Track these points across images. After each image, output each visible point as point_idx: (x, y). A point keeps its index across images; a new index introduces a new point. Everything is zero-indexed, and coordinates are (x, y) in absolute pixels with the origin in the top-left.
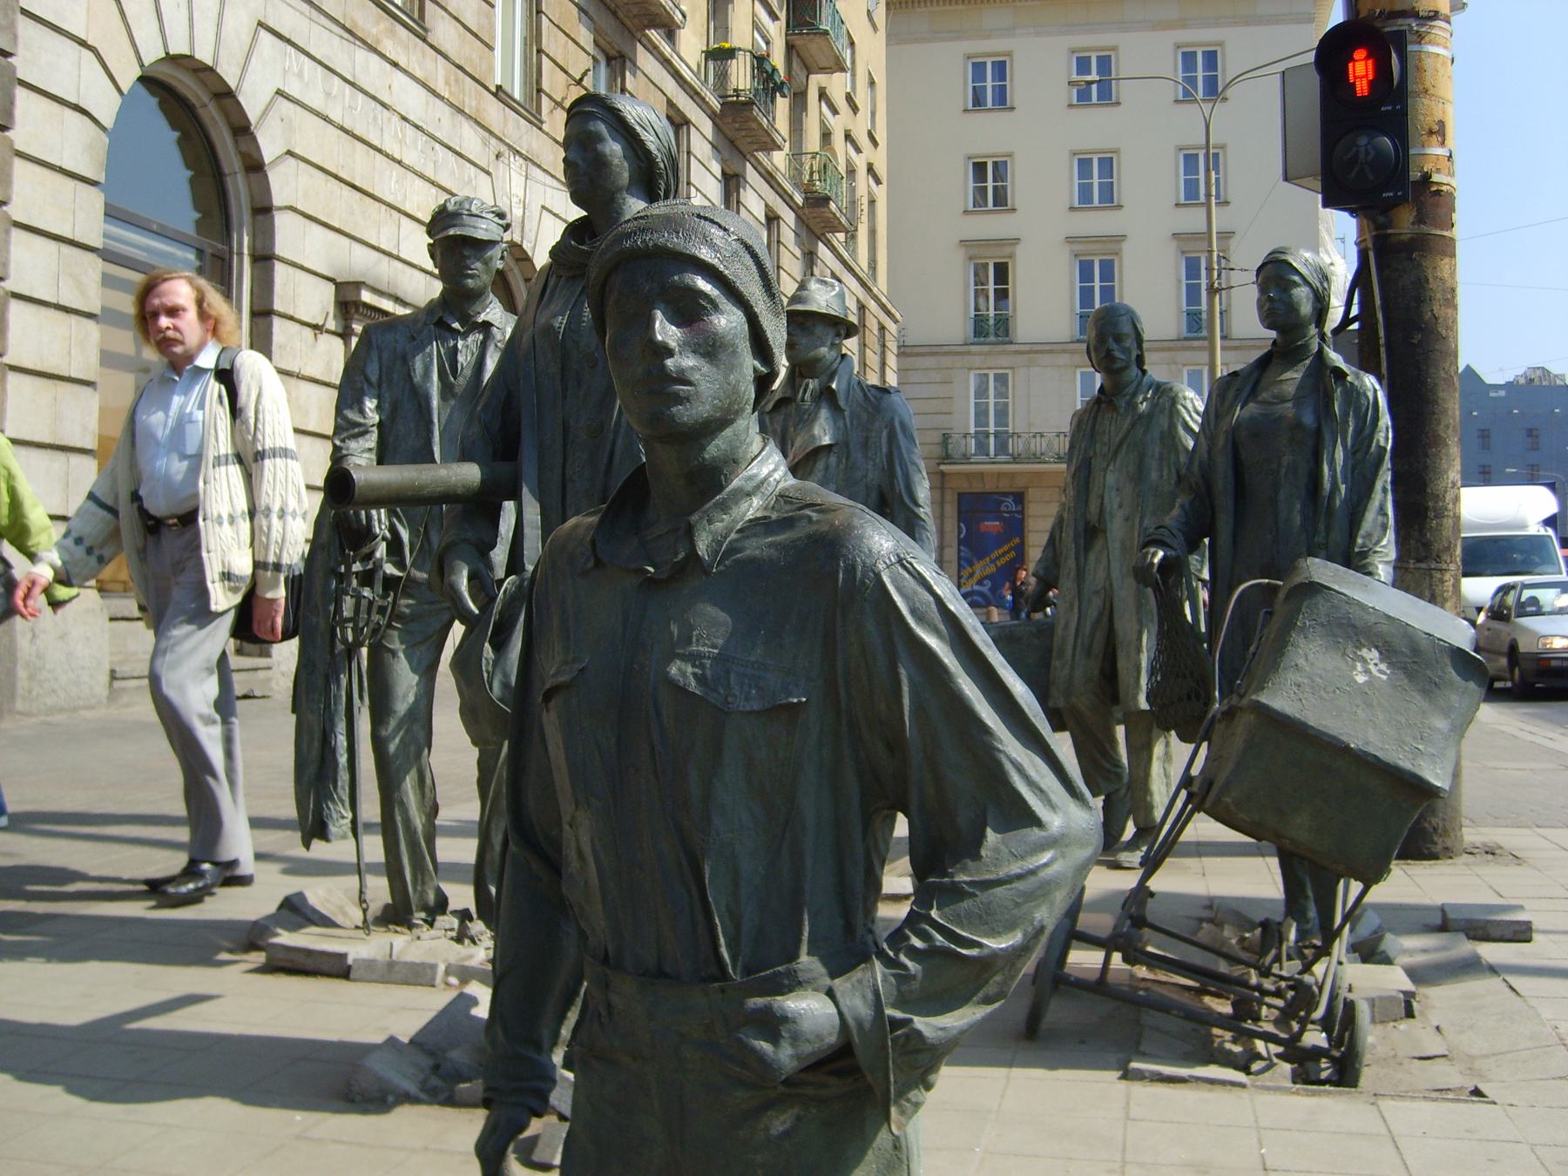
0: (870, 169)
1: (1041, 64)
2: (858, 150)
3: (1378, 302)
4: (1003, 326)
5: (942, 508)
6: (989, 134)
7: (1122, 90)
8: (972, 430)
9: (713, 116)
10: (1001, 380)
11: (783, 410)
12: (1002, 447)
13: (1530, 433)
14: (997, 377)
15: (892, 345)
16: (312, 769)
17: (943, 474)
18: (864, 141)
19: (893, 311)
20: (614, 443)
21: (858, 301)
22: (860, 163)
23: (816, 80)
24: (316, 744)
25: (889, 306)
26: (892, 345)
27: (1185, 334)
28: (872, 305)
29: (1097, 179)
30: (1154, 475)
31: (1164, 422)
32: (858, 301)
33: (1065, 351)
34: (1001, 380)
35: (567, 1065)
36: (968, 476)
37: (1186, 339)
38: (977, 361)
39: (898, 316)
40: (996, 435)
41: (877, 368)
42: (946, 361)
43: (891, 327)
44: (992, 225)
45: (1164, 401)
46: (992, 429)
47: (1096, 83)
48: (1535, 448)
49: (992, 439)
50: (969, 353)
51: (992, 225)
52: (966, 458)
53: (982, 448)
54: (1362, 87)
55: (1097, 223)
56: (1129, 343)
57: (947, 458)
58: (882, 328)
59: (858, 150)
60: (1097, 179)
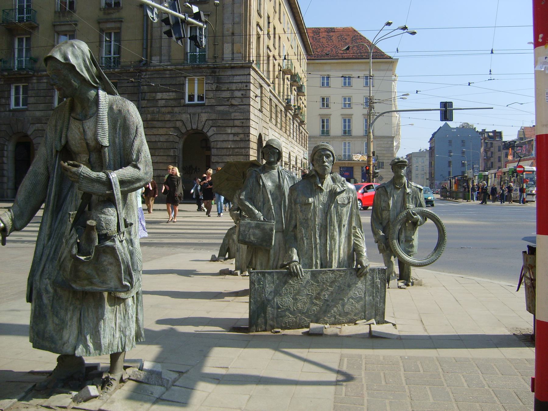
0: (274, 57)
1: (336, 82)
2: (270, 51)
4: (328, 133)
6: (325, 92)
7: (353, 106)
9: (284, 107)
13: (463, 141)
18: (277, 57)
22: (271, 54)
23: (286, 76)
29: (348, 103)
35: (541, 38)
38: (322, 139)
42: (316, 139)
44: (325, 111)
47: (347, 80)
48: (463, 146)
51: (325, 111)
55: (347, 111)
59: (270, 51)
60: (348, 103)
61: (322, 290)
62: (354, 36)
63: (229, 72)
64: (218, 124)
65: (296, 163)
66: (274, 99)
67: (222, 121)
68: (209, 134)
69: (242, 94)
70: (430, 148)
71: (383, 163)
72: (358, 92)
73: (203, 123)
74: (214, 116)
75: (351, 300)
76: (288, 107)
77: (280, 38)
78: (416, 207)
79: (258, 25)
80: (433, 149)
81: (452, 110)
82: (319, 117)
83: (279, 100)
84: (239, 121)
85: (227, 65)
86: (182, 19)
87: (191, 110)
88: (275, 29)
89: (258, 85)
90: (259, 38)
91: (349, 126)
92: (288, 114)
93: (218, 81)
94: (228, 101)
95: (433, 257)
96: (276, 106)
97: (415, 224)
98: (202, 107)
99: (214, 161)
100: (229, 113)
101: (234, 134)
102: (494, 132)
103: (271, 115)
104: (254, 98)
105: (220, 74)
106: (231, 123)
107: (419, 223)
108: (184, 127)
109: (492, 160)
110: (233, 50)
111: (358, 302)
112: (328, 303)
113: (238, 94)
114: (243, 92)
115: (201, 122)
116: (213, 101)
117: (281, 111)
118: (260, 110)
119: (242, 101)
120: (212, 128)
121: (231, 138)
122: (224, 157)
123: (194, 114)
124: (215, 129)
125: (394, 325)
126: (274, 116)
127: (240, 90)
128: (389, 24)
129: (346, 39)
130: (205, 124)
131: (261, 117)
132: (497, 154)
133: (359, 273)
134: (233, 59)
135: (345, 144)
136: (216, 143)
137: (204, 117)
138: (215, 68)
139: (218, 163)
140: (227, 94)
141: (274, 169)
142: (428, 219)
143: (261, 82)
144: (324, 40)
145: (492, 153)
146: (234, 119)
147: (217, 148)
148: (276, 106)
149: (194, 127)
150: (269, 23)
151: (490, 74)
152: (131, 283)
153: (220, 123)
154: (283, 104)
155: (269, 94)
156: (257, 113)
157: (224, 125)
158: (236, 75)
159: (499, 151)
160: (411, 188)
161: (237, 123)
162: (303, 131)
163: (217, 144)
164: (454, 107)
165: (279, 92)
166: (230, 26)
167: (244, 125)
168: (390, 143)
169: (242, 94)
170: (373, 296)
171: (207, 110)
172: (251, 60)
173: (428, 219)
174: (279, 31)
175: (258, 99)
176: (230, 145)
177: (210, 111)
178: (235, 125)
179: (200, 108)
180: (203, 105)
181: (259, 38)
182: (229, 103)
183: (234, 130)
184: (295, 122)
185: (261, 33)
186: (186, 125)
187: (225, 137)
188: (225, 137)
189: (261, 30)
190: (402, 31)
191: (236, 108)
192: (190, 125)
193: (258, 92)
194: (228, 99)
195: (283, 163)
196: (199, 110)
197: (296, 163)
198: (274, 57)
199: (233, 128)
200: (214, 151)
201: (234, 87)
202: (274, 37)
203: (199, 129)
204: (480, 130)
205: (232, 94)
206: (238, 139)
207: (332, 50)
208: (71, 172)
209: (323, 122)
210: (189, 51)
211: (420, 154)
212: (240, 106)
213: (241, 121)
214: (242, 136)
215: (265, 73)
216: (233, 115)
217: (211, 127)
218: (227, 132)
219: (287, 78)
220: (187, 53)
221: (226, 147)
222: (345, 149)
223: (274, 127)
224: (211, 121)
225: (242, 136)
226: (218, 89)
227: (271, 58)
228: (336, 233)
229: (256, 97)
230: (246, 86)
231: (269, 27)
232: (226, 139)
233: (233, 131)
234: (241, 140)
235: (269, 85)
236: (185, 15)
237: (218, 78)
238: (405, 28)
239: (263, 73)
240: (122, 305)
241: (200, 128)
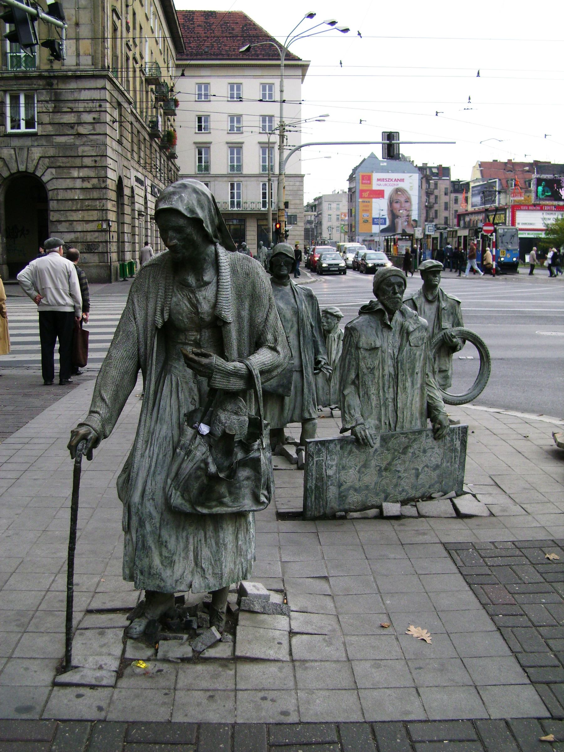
0: (134, 59)
2: (130, 50)
9: (149, 134)
22: (131, 54)
34: (239, 185)
61: (393, 459)
62: (246, 25)
63: (73, 85)
64: (58, 164)
65: (146, 208)
66: (136, 124)
67: (64, 159)
68: (45, 179)
69: (94, 119)
70: (350, 189)
71: (295, 217)
72: (252, 111)
73: (35, 162)
74: (51, 152)
75: (426, 469)
76: (154, 135)
77: (141, 28)
78: (453, 326)
79: (114, 10)
80: (353, 190)
81: (399, 144)
82: (194, 146)
83: (142, 125)
84: (90, 159)
85: (70, 74)
86: (31, 14)
87: (16, 142)
88: (134, 14)
89: (115, 105)
90: (115, 29)
91: (239, 160)
92: (154, 145)
93: (57, 100)
94: (72, 128)
95: (475, 392)
96: (138, 132)
97: (454, 348)
98: (34, 138)
99: (54, 220)
100: (73, 147)
101: (83, 179)
102: (440, 168)
103: (132, 147)
104: (111, 123)
105: (59, 87)
106: (78, 162)
107: (458, 347)
108: (5, 169)
109: (436, 207)
110: (77, 49)
111: (435, 469)
112: (400, 474)
113: (88, 118)
114: (96, 115)
115: (32, 161)
116: (50, 129)
117: (145, 139)
118: (120, 142)
119: (94, 129)
120: (50, 170)
121: (78, 184)
122: (69, 214)
123: (21, 149)
124: (53, 171)
125: (474, 496)
126: (136, 148)
127: (90, 112)
128: (311, 16)
129: (233, 29)
130: (38, 163)
131: (120, 151)
132: (443, 199)
133: (437, 435)
134: (78, 64)
135: (232, 185)
136: (55, 192)
137: (37, 153)
138: (50, 77)
139: (60, 222)
140: (70, 118)
141: (286, 285)
142: (467, 342)
143: (121, 99)
144: (200, 30)
145: (436, 197)
146: (83, 156)
147: (57, 200)
148: (138, 132)
149: (22, 168)
150: (127, 6)
151: (469, 102)
152: (269, 499)
153: (61, 162)
154: (148, 129)
155: (131, 118)
156: (115, 145)
157: (68, 165)
158: (85, 89)
159: (446, 194)
160: (447, 301)
161: (88, 161)
162: (173, 167)
163: (57, 194)
164: (401, 140)
165: (142, 112)
166: (73, 12)
167: (97, 165)
168: (298, 184)
169: (94, 119)
170: (451, 462)
171: (40, 142)
172: (106, 65)
173: (467, 342)
174: (140, 18)
175: (116, 125)
176: (77, 195)
177: (45, 144)
178: (84, 164)
179: (30, 138)
180: (35, 135)
181: (115, 29)
182: (74, 132)
183: (83, 173)
184: (162, 155)
185: (118, 23)
186: (10, 166)
187: (69, 183)
188: (69, 183)
189: (119, 18)
190: (330, 27)
191: (85, 139)
192: (14, 165)
193: (116, 114)
194: (71, 126)
195: (136, 213)
196: (28, 142)
197: (146, 208)
198: (134, 59)
199: (81, 170)
200: (53, 205)
201: (81, 107)
202: (134, 28)
203: (29, 171)
204: (420, 165)
205: (79, 117)
206: (89, 186)
207: (213, 46)
208: (202, 366)
209: (200, 153)
210: (8, 51)
211: (335, 198)
212: (91, 137)
213: (94, 158)
214: (95, 181)
215: (125, 84)
216: (80, 149)
217: (48, 168)
218: (72, 176)
219: (152, 90)
220: (6, 53)
221: (72, 198)
222: (232, 193)
223: (137, 166)
224: (47, 160)
225: (95, 181)
226: (57, 111)
227: (131, 61)
228: (409, 384)
229: (114, 122)
230: (100, 106)
231: (127, 13)
232: (71, 186)
233: (81, 175)
234: (94, 188)
235: (130, 103)
236: (36, 9)
237: (56, 94)
238: (333, 23)
239: (121, 84)
240: (243, 520)
241: (31, 170)
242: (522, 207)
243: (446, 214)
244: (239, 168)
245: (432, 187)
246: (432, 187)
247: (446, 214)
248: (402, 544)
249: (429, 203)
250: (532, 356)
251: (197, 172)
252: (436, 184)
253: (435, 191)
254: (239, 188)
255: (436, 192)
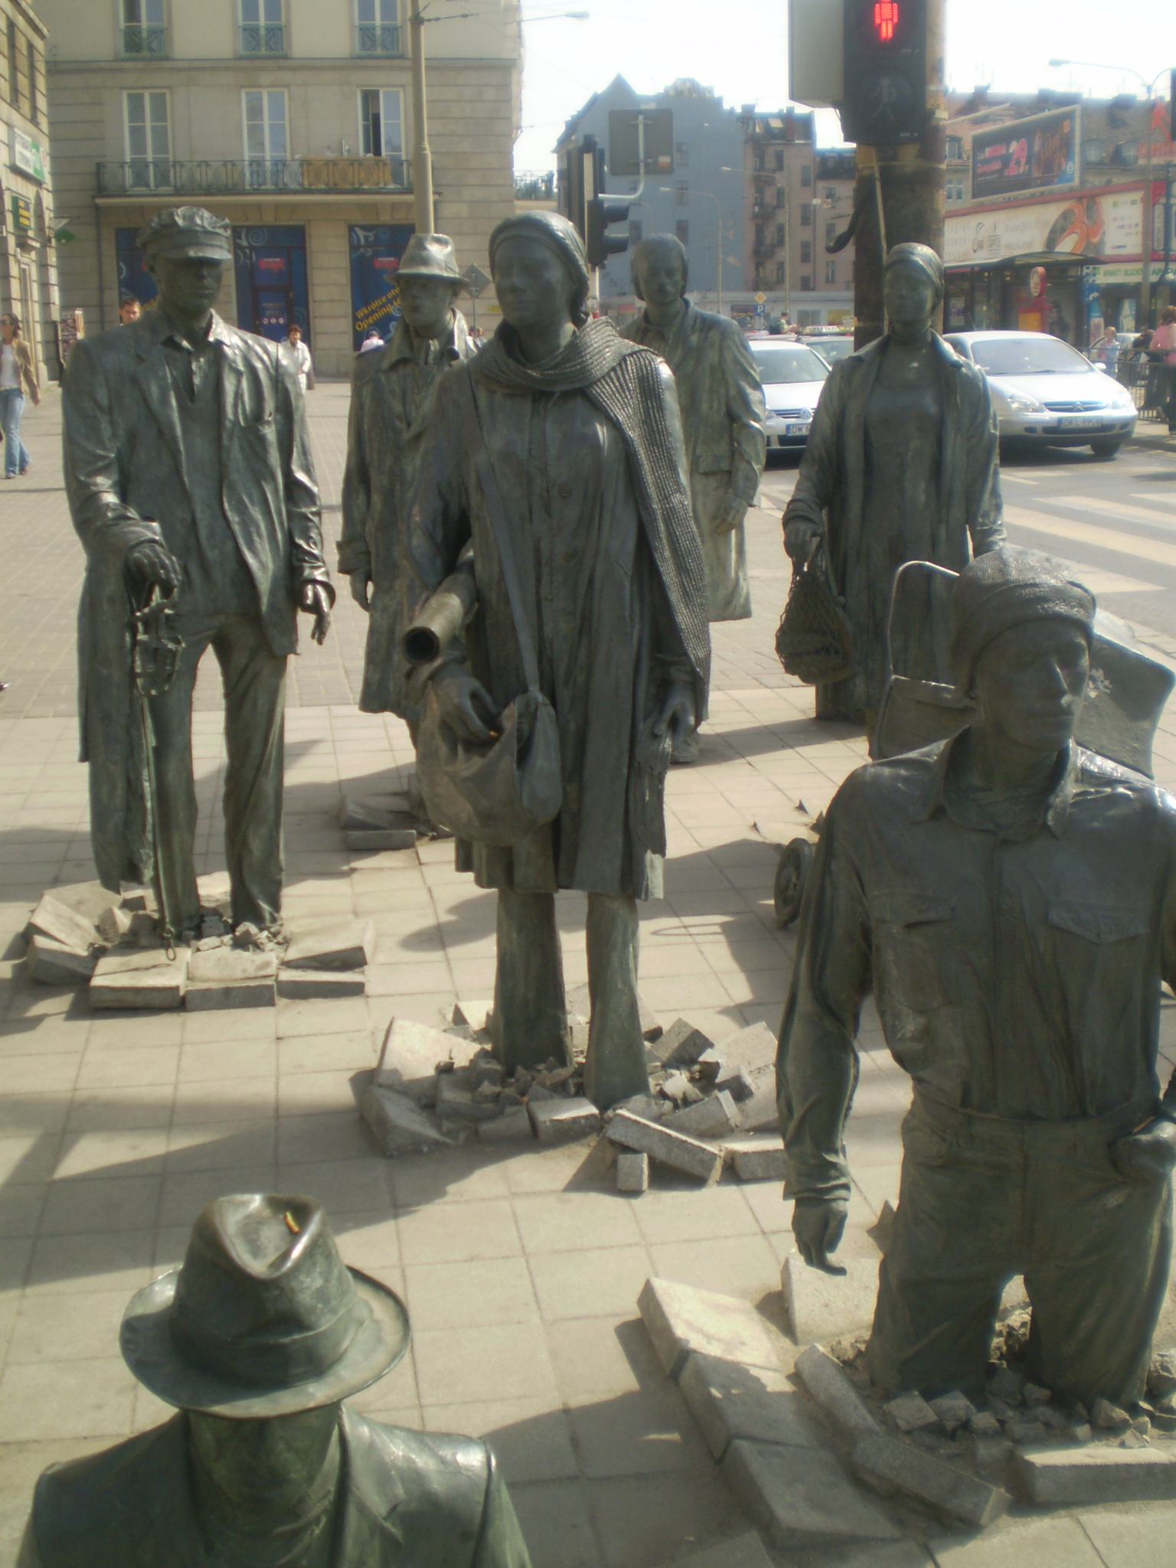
3: (883, 231)
5: (99, 247)
8: (128, 158)
10: (159, 102)
11: (401, 370)
12: (163, 178)
14: (153, 97)
15: (41, 66)
16: (117, 818)
17: (97, 208)
19: (41, 25)
20: (593, 570)
21: (8, 18)
24: (120, 792)
25: (37, 21)
26: (41, 66)
27: (358, 51)
28: (20, 21)
30: (705, 407)
31: (713, 356)
32: (8, 18)
33: (227, 69)
34: (159, 102)
36: (128, 210)
37: (360, 58)
39: (45, 31)
40: (156, 165)
41: (27, 93)
43: (39, 44)
45: (714, 335)
46: (150, 157)
49: (151, 168)
50: (121, 70)
52: (123, 192)
53: (140, 178)
54: (887, 31)
56: (678, 277)
57: (101, 190)
58: (31, 47)
109: (782, 217)
242: (361, 500)
243: (804, 234)
244: (277, 34)
245: (770, 162)
246: (770, 162)
247: (804, 234)
248: (764, 1233)
249: (761, 205)
250: (1099, 1461)
251: (123, 54)
252: (779, 157)
253: (777, 176)
254: (160, 113)
255: (780, 180)
